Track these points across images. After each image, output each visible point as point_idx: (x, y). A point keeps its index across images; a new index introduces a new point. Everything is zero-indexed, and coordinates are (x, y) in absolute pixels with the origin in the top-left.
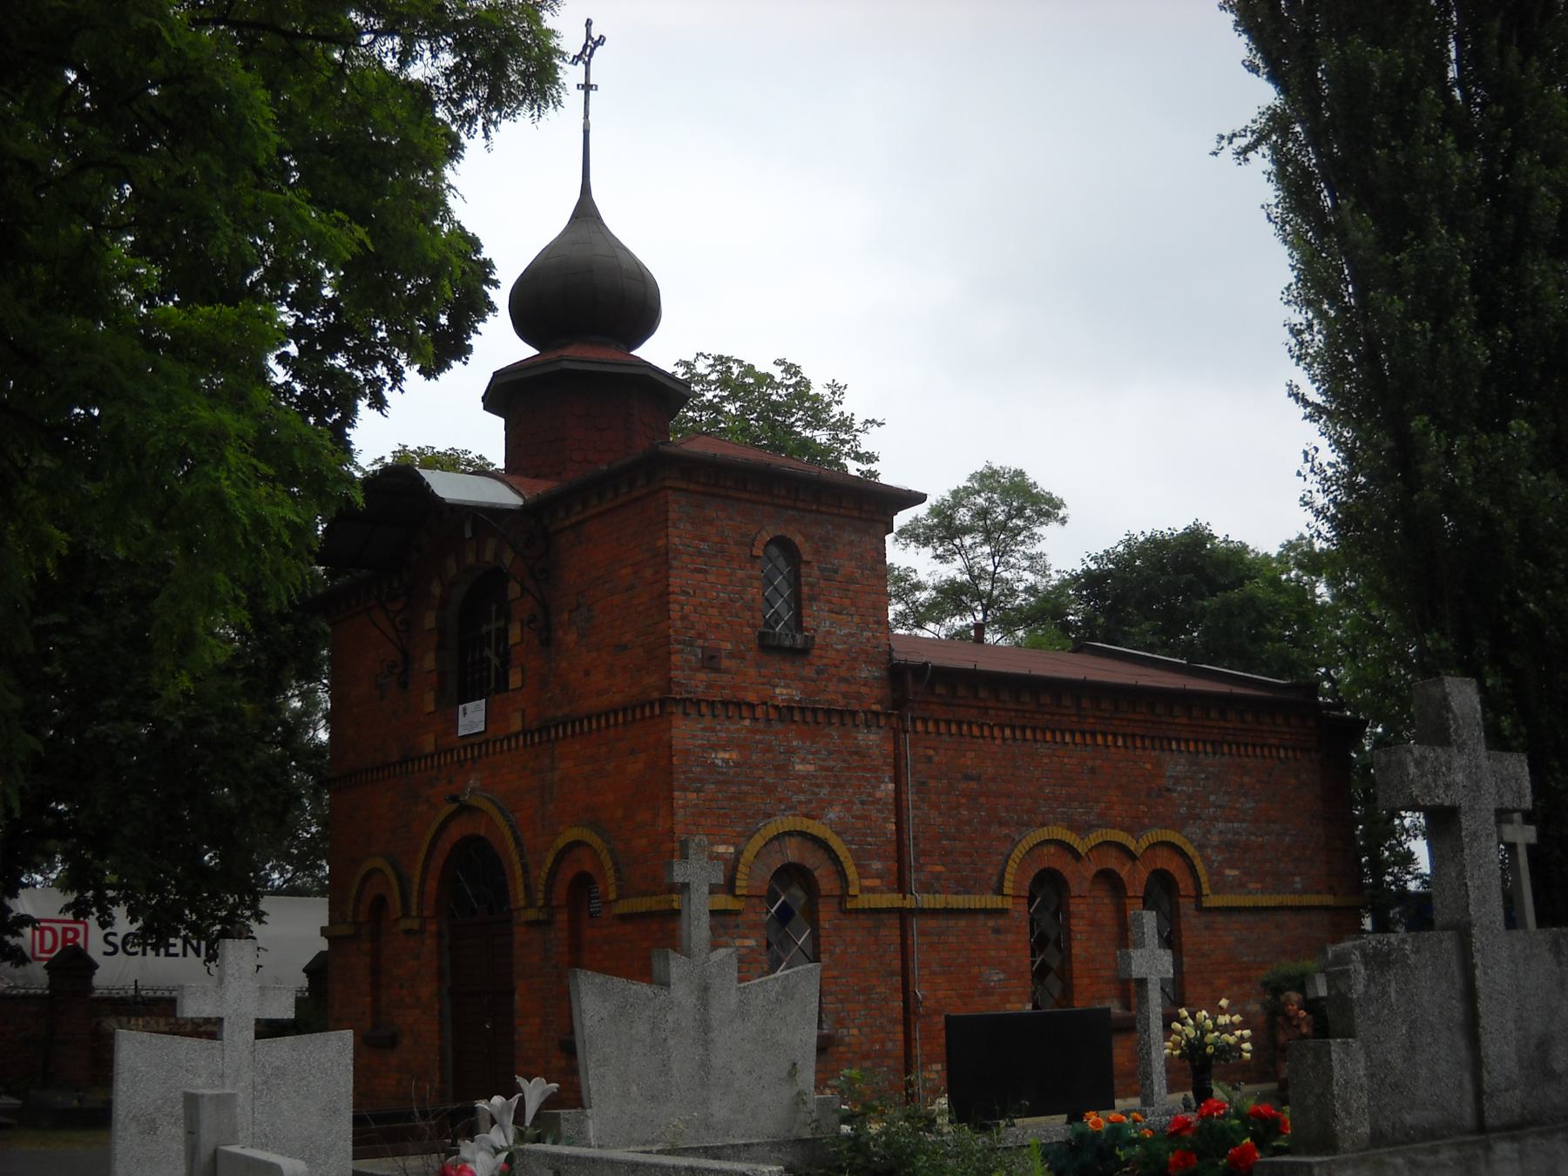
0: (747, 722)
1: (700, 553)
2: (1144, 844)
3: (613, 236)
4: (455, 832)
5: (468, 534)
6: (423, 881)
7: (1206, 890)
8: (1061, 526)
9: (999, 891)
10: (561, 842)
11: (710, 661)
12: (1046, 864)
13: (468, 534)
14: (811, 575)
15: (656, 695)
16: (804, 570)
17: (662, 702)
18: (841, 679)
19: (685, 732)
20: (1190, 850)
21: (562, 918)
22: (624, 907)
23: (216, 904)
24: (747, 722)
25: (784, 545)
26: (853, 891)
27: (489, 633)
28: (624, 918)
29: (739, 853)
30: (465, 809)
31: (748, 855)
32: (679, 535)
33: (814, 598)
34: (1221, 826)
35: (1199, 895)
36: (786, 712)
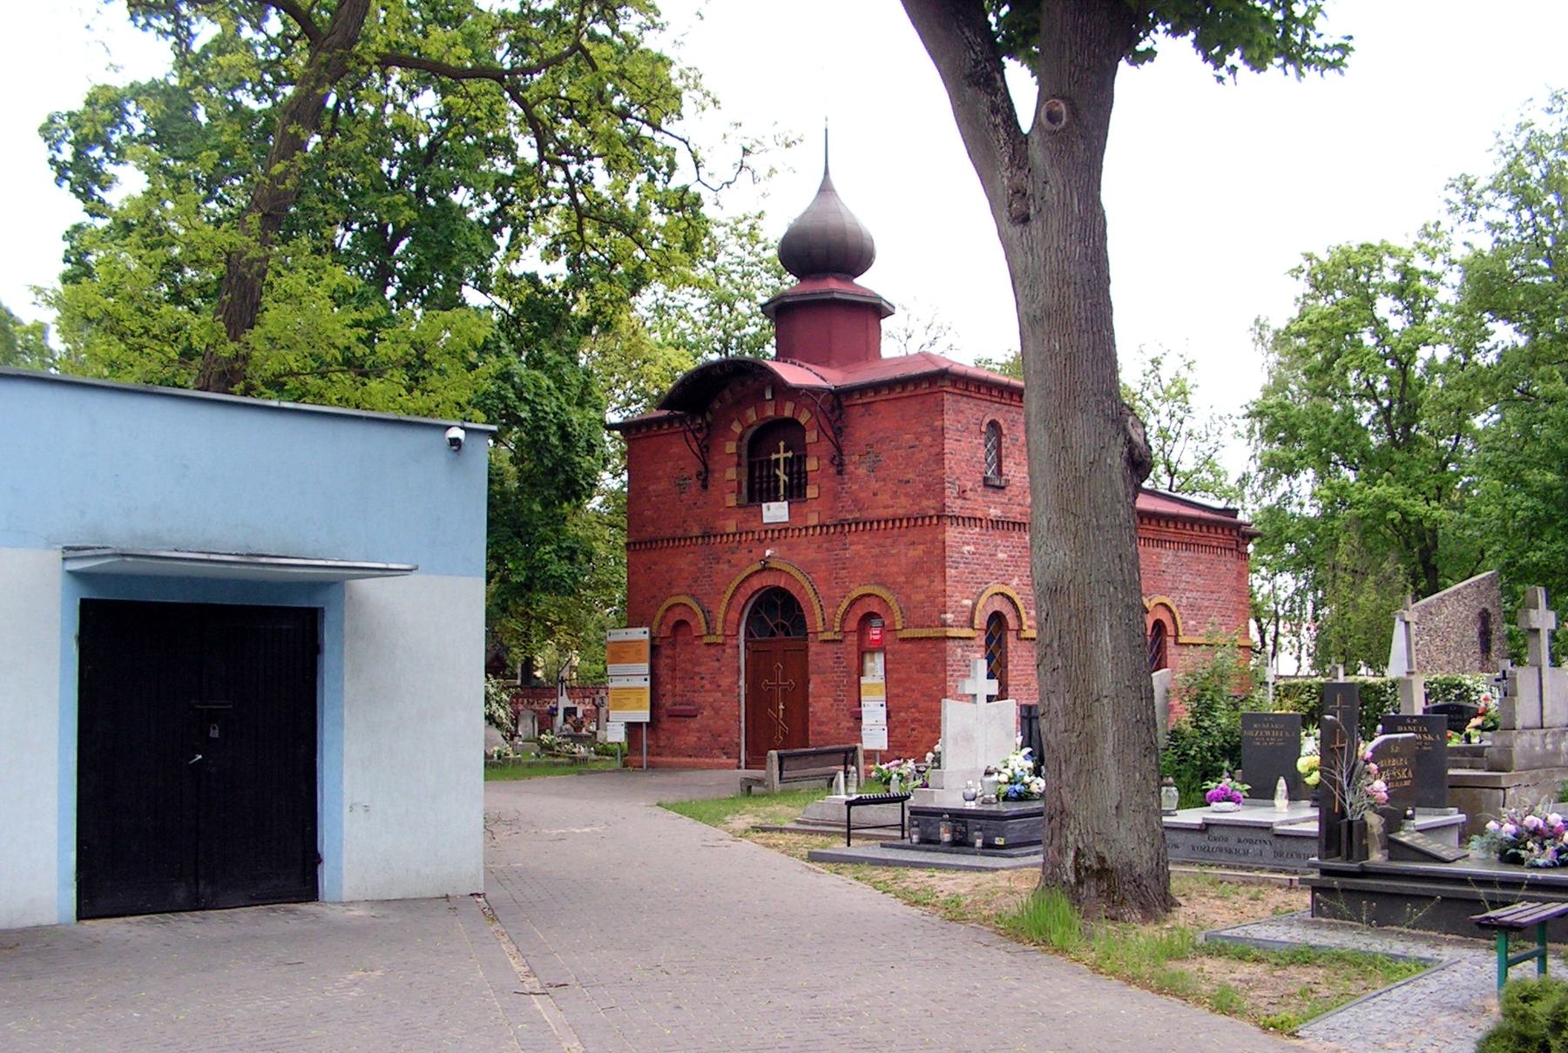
0: (978, 529)
1: (958, 430)
2: (1153, 603)
3: (1018, 278)
4: (756, 583)
5: (769, 396)
6: (726, 613)
7: (1181, 633)
8: (39, 125)
9: (972, 626)
10: (855, 594)
11: (962, 494)
12: (997, 608)
13: (769, 396)
14: (1006, 442)
15: (932, 512)
16: (1003, 440)
17: (939, 517)
18: (1019, 505)
19: (952, 534)
20: (1174, 608)
21: (854, 638)
22: (906, 634)
23: (1291, 631)
24: (978, 529)
25: (993, 424)
26: (1025, 627)
27: (777, 460)
28: (904, 640)
29: (974, 606)
30: (766, 568)
31: (980, 606)
32: (949, 420)
33: (1007, 456)
34: (1187, 594)
35: (1177, 635)
36: (996, 524)
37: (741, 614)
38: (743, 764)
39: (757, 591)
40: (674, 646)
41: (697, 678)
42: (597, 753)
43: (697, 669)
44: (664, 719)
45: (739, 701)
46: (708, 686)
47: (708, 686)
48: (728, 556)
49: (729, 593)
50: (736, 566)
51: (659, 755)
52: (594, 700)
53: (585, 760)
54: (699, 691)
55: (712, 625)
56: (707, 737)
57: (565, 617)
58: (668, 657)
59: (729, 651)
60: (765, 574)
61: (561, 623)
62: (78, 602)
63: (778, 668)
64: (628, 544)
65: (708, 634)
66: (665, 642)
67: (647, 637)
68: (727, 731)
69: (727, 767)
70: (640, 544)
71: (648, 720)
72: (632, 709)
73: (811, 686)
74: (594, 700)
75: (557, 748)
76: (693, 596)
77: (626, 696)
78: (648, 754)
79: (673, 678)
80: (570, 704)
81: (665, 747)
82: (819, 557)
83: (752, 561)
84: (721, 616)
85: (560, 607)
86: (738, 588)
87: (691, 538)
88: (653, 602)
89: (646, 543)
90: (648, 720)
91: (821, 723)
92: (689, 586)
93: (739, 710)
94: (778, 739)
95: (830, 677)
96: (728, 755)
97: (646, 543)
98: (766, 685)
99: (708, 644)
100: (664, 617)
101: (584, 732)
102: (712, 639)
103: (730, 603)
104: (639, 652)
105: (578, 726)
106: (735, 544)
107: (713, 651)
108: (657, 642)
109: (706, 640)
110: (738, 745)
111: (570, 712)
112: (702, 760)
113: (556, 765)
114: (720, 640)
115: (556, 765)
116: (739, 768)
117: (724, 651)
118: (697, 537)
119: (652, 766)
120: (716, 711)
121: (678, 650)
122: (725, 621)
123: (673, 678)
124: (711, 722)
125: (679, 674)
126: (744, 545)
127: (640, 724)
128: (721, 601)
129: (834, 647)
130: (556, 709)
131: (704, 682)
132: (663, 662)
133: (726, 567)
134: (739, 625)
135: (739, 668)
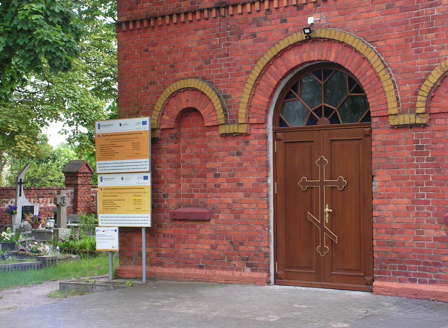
37: (272, 97)
38: (272, 279)
39: (292, 70)
40: (177, 137)
41: (210, 175)
42: (62, 250)
43: (210, 165)
44: (166, 223)
45: (268, 203)
46: (225, 185)
47: (225, 185)
48: (253, 29)
49: (253, 76)
50: (262, 40)
51: (161, 264)
52: (55, 200)
53: (53, 261)
54: (213, 191)
55: (231, 112)
56: (224, 246)
57: (24, 127)
58: (171, 152)
59: (254, 142)
60: (307, 47)
61: (20, 131)
62: (252, 272)
63: (322, 162)
64: (118, 24)
65: (226, 123)
66: (167, 135)
67: (147, 128)
68: (251, 239)
69: (254, 282)
70: (134, 22)
71: (148, 224)
72: (128, 211)
73: (376, 185)
74: (55, 200)
75: (21, 247)
76: (204, 79)
77: (120, 197)
78: (147, 264)
79: (178, 176)
80: (27, 203)
81: (166, 256)
82: (391, 19)
83: (287, 33)
84: (245, 100)
85: (19, 118)
86: (267, 66)
87: (202, 11)
88: (152, 89)
89: (141, 21)
90: (148, 224)
91: (392, 232)
92: (199, 68)
93: (268, 214)
94: (323, 249)
95: (406, 172)
96: (254, 268)
97: (141, 21)
98: (304, 183)
99: (225, 136)
100: (166, 105)
101: (40, 228)
102: (232, 129)
103: (256, 85)
104: (136, 146)
105: (35, 223)
106: (262, 13)
107: (231, 143)
108: (158, 134)
109: (223, 130)
110: (267, 255)
111: (27, 210)
112: (218, 272)
113: (25, 268)
114: (243, 129)
115: (25, 268)
116: (269, 283)
117: (247, 143)
118: (210, 10)
119: (151, 277)
120: (237, 214)
121: (183, 142)
122: (249, 107)
123: (178, 176)
124: (229, 228)
125: (183, 171)
126: (275, 14)
127: (138, 230)
128: (243, 84)
129: (413, 134)
130: (15, 208)
131: (220, 180)
132: (164, 157)
133: (250, 41)
134: (267, 111)
135: (267, 162)
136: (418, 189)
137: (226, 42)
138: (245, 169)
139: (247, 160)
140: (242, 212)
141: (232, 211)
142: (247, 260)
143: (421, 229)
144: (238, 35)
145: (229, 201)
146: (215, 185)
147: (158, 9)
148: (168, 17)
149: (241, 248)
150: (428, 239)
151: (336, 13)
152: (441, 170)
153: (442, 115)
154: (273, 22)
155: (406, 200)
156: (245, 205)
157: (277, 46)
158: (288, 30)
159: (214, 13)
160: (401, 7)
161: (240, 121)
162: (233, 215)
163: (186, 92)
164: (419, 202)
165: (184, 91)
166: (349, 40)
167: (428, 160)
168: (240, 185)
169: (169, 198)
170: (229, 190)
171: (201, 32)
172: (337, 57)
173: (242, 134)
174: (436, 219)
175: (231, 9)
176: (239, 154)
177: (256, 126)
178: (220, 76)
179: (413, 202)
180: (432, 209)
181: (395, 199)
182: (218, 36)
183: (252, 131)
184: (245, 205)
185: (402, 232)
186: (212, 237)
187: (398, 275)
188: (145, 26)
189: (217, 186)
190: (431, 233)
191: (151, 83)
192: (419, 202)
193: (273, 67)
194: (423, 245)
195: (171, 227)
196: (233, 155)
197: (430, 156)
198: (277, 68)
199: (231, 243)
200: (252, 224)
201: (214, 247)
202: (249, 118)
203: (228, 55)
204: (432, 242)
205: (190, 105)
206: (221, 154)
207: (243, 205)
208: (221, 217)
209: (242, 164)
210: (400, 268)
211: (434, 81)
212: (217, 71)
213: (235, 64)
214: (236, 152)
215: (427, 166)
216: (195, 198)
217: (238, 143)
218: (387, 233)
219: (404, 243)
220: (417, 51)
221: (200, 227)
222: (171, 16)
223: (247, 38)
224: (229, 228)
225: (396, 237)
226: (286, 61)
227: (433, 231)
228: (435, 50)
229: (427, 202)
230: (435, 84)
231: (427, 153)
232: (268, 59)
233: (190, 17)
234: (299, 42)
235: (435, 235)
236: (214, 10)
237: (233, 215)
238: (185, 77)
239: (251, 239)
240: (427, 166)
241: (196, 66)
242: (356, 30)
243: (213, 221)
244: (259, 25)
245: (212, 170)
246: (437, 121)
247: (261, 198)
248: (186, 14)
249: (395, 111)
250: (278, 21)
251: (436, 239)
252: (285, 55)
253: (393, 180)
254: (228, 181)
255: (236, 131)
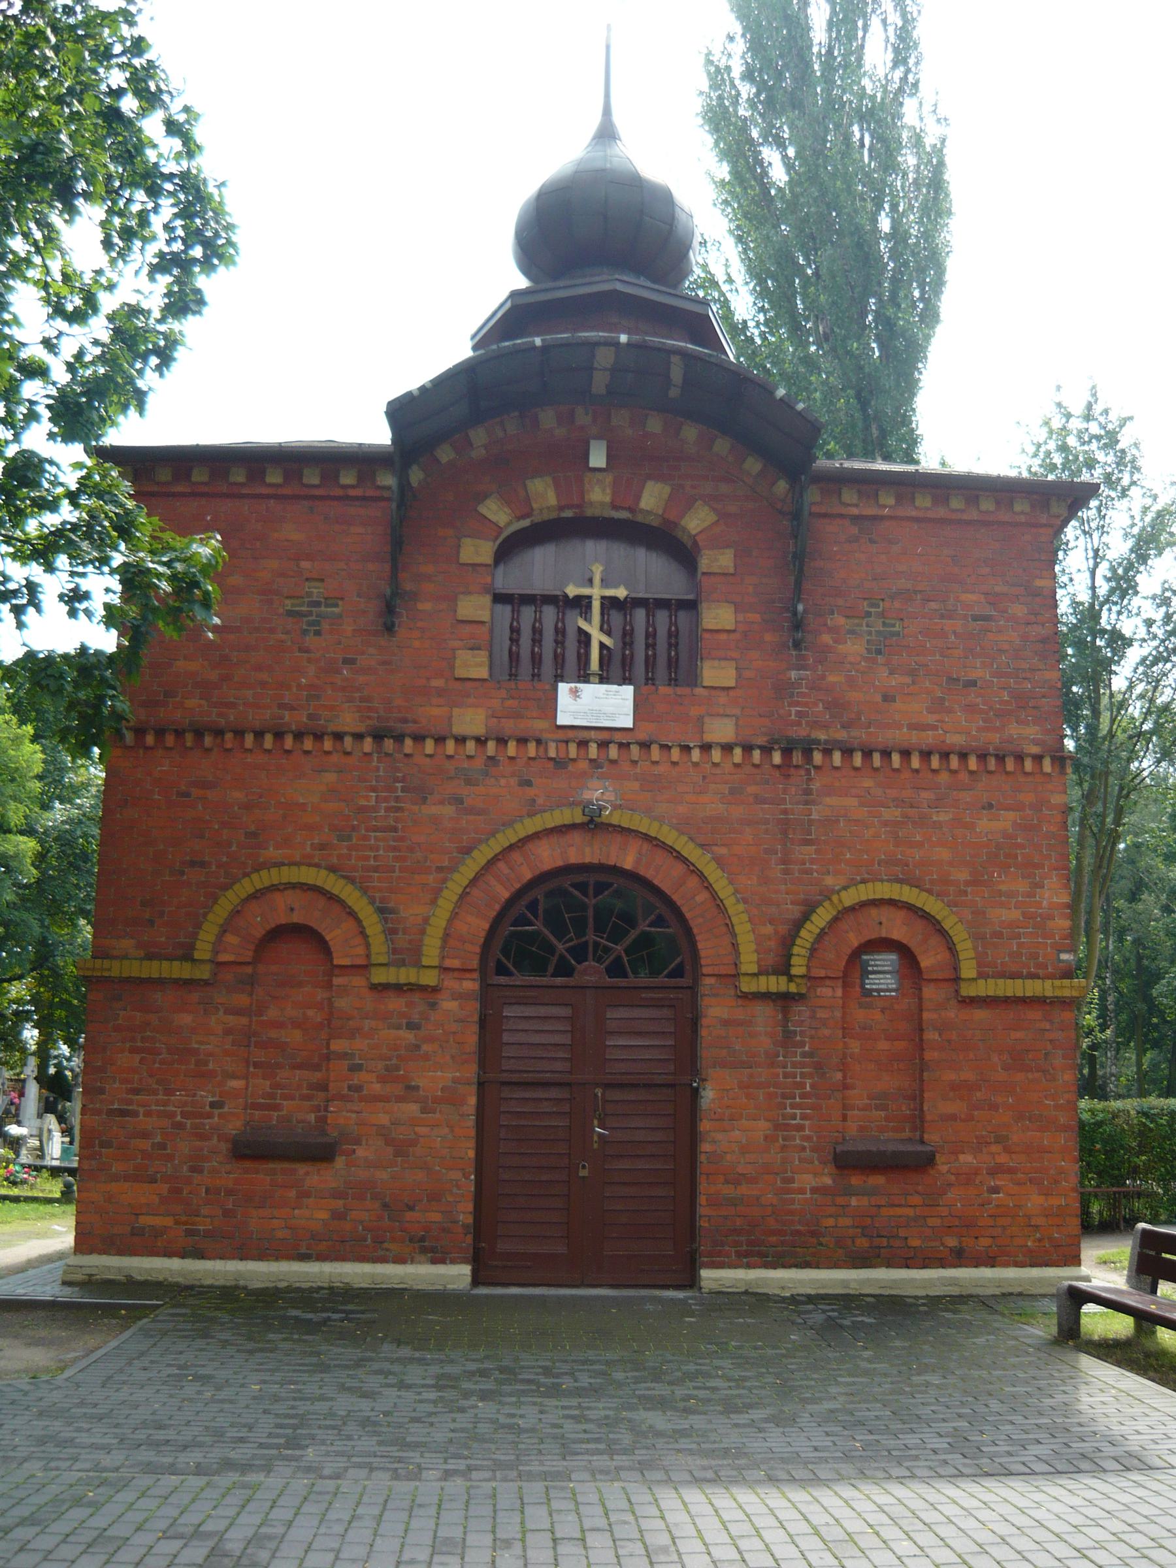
43: (338, 1045)
54: (343, 1098)
60: (576, 837)
73: (708, 1095)
76: (332, 869)
92: (322, 847)
106: (479, 763)
107: (395, 1003)
114: (429, 978)
117: (433, 1006)
118: (359, 737)
122: (446, 936)
124: (383, 1175)
131: (357, 1078)
133: (448, 810)
136: (785, 1104)
137: (393, 804)
138: (426, 1057)
139: (430, 1039)
140: (413, 1143)
141: (389, 1142)
142: (422, 1239)
143: (789, 1174)
144: (421, 794)
145: (384, 1119)
146: (350, 1088)
147: (220, 715)
148: (252, 735)
149: (409, 1215)
150: (802, 1191)
151: (636, 785)
152: (825, 1073)
153: (828, 982)
154: (503, 782)
155: (762, 1124)
156: (422, 1130)
157: (518, 826)
158: (534, 801)
159: (368, 744)
160: (756, 796)
161: (425, 961)
162: (390, 1150)
163: (289, 892)
164: (787, 1127)
165: (285, 889)
166: (669, 836)
167: (804, 1055)
168: (409, 1088)
169: (226, 1109)
170: (386, 1099)
171: (331, 777)
172: (638, 861)
173: (423, 989)
174: (816, 1155)
175: (408, 742)
176: (411, 1026)
177: (456, 974)
178: (376, 869)
179: (777, 1127)
180: (808, 1138)
181: (744, 1121)
182: (374, 789)
183: (446, 983)
184: (422, 1130)
185: (752, 1180)
186: (338, 1195)
187: (745, 1257)
188: (189, 744)
189: (358, 1088)
190: (807, 1180)
191: (192, 864)
192: (787, 1127)
193: (501, 865)
194: (792, 1201)
195: (229, 1173)
196: (399, 1027)
197: (807, 1048)
198: (512, 868)
199: (385, 1206)
200: (438, 1168)
201: (338, 1216)
202: (217, 953)
203: (395, 829)
204: (808, 1196)
205: (296, 918)
206: (367, 1024)
207: (417, 1129)
208: (361, 1152)
209: (418, 1047)
210: (750, 1243)
211: (822, 924)
212: (367, 858)
213: (411, 849)
214: (404, 1021)
215: (803, 1065)
216: (284, 1112)
217: (410, 1004)
218: (727, 1182)
219: (758, 1199)
220: (786, 872)
221: (307, 1173)
222: (259, 735)
223: (442, 802)
224: (383, 1175)
225: (744, 1189)
226: (532, 857)
227: (810, 1176)
228: (815, 874)
229: (800, 1128)
230: (822, 929)
231: (803, 1044)
232: (498, 849)
233: (308, 744)
234: (565, 826)
235: (814, 1184)
236: (369, 740)
237: (390, 1150)
238: (323, 863)
239: (435, 1197)
240: (803, 1065)
241: (316, 841)
242: (675, 821)
243: (340, 1162)
244: (469, 782)
245: (344, 1056)
246: (819, 990)
247: (462, 1115)
248: (299, 736)
249: (383, 959)
250: (513, 781)
251: (814, 1190)
252: (530, 846)
253: (740, 1088)
254: (382, 1080)
255: (413, 980)
